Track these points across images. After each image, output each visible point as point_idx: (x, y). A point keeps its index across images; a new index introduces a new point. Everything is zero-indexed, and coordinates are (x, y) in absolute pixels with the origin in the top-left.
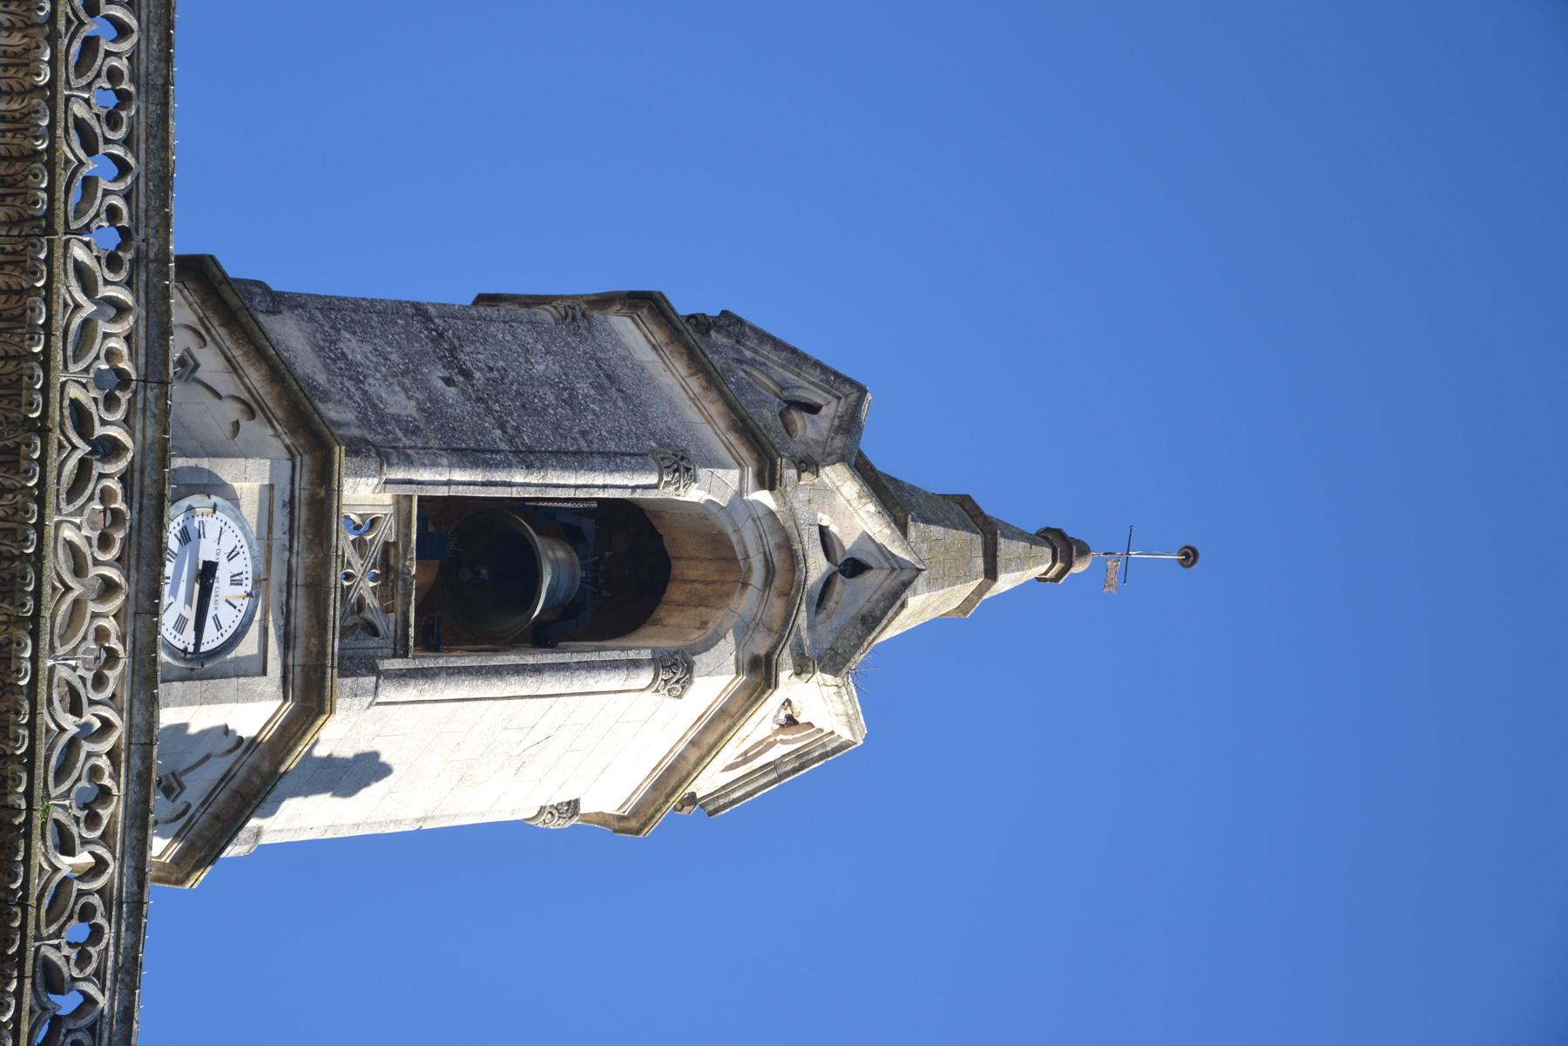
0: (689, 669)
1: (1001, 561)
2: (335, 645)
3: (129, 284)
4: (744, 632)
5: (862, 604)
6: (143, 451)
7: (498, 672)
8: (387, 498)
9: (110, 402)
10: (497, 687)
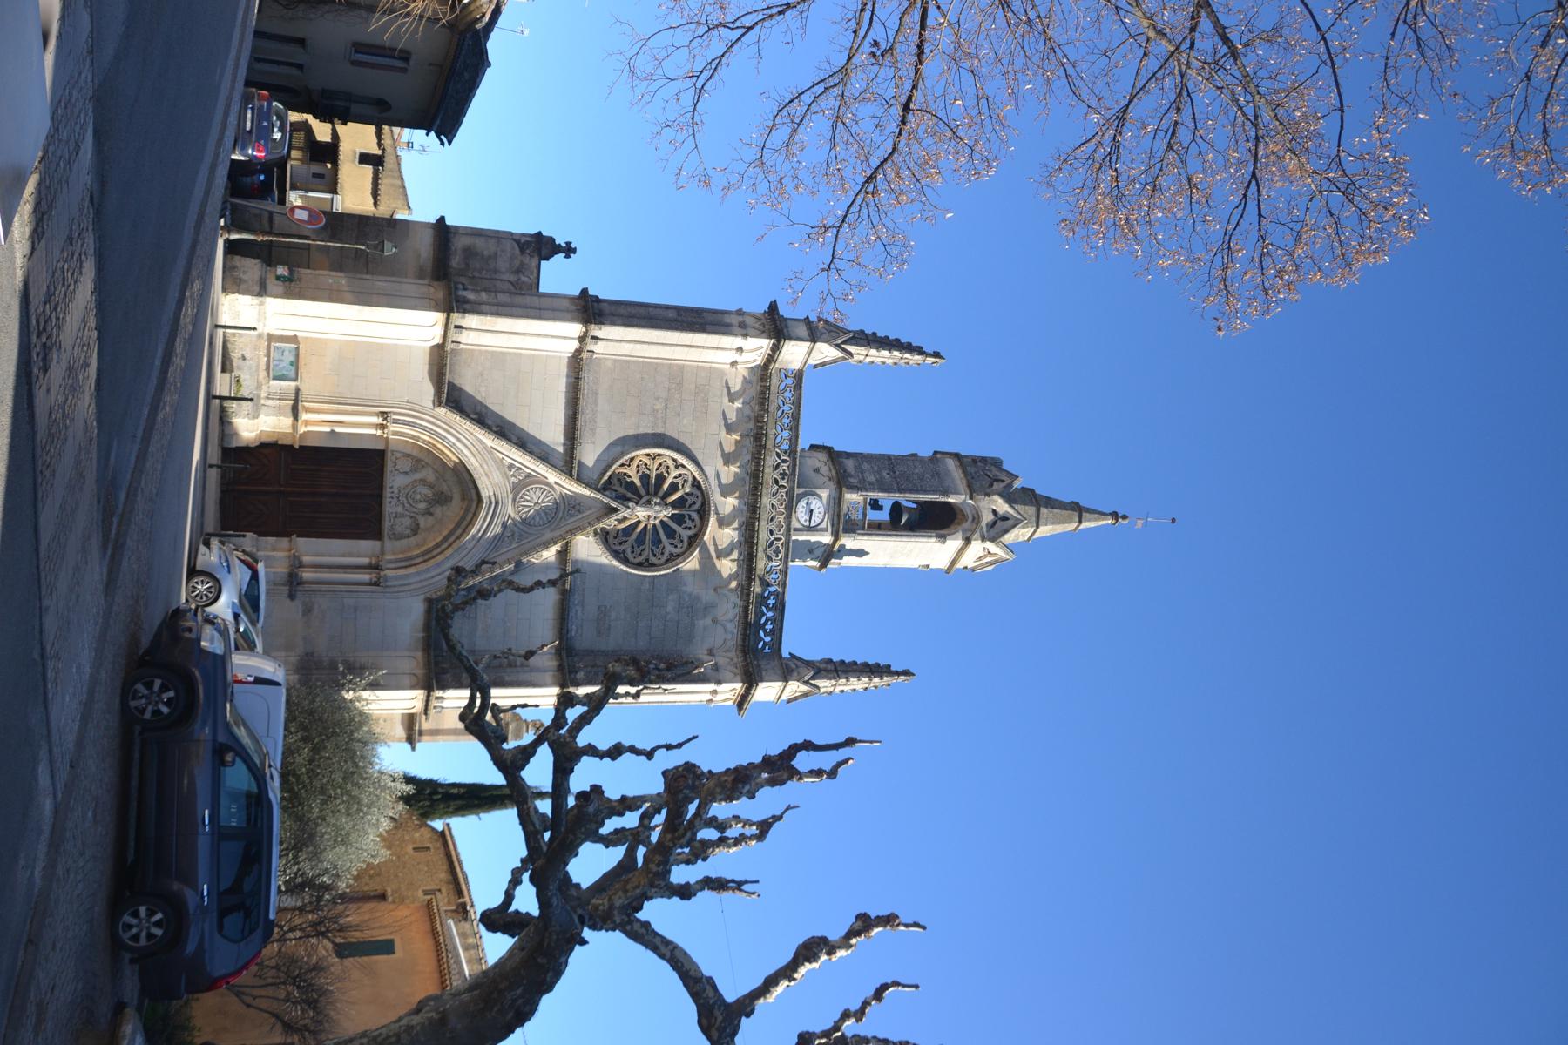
0: (945, 538)
1: (1083, 520)
2: (841, 527)
3: (789, 456)
4: (964, 531)
5: (1005, 528)
6: (790, 487)
7: (890, 535)
8: (862, 498)
9: (783, 479)
10: (889, 538)
